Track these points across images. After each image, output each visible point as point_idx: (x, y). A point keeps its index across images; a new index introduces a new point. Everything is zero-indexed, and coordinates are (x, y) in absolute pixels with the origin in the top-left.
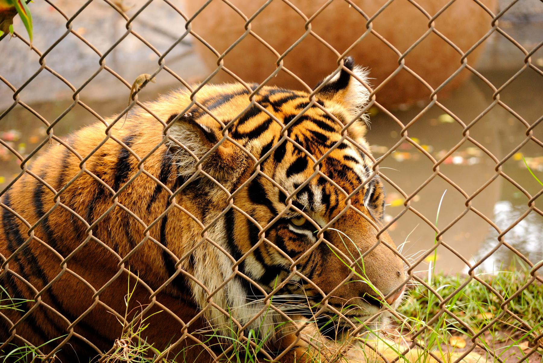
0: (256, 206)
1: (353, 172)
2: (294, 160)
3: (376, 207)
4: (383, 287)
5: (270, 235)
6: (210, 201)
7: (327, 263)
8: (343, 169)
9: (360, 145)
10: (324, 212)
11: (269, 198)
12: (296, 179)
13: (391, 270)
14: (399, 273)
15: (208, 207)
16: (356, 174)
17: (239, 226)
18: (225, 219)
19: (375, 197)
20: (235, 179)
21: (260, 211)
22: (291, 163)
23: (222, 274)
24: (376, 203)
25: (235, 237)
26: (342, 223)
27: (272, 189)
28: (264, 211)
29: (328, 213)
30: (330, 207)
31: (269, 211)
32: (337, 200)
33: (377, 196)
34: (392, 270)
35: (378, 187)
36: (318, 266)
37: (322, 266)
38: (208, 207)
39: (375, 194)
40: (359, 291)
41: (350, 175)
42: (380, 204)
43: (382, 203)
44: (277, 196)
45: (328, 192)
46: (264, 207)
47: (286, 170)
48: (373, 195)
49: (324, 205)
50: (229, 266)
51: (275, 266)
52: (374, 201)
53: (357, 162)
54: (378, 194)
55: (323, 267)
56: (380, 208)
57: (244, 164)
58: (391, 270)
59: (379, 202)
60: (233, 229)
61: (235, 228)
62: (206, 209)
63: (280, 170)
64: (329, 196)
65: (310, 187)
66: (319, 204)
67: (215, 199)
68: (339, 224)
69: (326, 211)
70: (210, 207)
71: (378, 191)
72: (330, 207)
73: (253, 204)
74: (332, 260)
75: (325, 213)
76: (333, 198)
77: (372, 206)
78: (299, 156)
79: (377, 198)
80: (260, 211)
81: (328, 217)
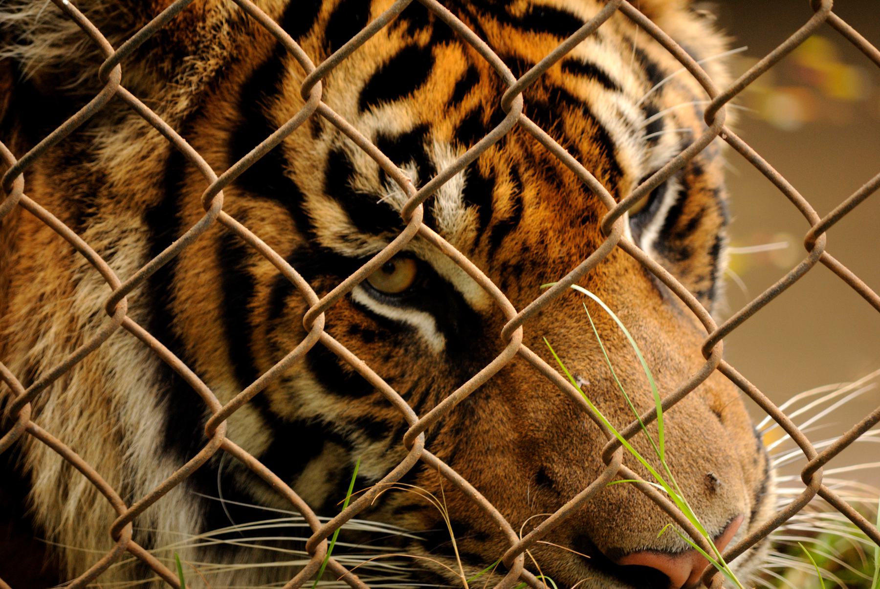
0: (252, 204)
1: (587, 112)
2: (393, 53)
3: (685, 255)
4: (650, 522)
5: (285, 311)
6: (102, 178)
7: (476, 423)
8: (552, 99)
9: (687, 49)
10: (472, 235)
11: (293, 177)
12: (385, 120)
13: (686, 466)
14: (712, 479)
15: (98, 201)
16: (595, 121)
17: (194, 266)
18: (149, 240)
19: (685, 219)
20: (183, 103)
21: (263, 219)
22: (380, 60)
23: (120, 436)
24: (687, 242)
25: (177, 307)
26: (530, 287)
27: (308, 146)
28: (275, 223)
29: (485, 238)
30: (494, 222)
31: (290, 224)
32: (518, 203)
33: (693, 215)
34: (691, 466)
35: (698, 186)
36: (443, 431)
37: (457, 430)
38: (98, 201)
39: (687, 210)
40: (573, 527)
41: (574, 123)
42: (702, 247)
43: (710, 242)
44: (320, 175)
45: (485, 171)
46: (277, 209)
47: (360, 85)
48: (675, 213)
49: (469, 209)
50: (148, 410)
51: (304, 421)
52: (682, 236)
53: (608, 83)
54: (697, 209)
55: (462, 436)
56: (701, 261)
57: (223, 47)
58: (686, 466)
59: (701, 239)
60: (173, 275)
61: (180, 276)
62: (90, 206)
63: (341, 83)
64: (491, 182)
65: (426, 148)
66: (453, 205)
67: (118, 175)
68: (520, 289)
69: (480, 231)
70: (104, 201)
71: (697, 200)
72: (494, 222)
73: (241, 195)
74: (492, 413)
75: (477, 242)
76: (504, 191)
77: (671, 249)
78: (409, 40)
79: (694, 224)
80: (263, 219)
81: (484, 259)
